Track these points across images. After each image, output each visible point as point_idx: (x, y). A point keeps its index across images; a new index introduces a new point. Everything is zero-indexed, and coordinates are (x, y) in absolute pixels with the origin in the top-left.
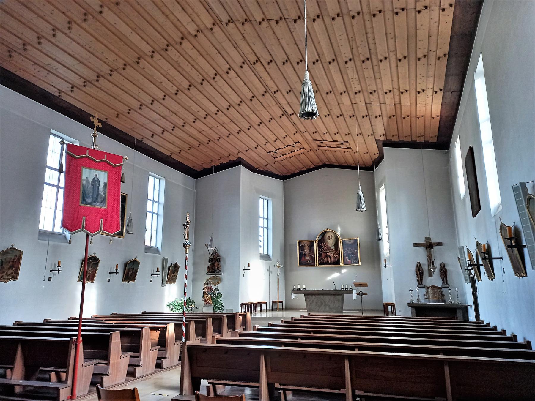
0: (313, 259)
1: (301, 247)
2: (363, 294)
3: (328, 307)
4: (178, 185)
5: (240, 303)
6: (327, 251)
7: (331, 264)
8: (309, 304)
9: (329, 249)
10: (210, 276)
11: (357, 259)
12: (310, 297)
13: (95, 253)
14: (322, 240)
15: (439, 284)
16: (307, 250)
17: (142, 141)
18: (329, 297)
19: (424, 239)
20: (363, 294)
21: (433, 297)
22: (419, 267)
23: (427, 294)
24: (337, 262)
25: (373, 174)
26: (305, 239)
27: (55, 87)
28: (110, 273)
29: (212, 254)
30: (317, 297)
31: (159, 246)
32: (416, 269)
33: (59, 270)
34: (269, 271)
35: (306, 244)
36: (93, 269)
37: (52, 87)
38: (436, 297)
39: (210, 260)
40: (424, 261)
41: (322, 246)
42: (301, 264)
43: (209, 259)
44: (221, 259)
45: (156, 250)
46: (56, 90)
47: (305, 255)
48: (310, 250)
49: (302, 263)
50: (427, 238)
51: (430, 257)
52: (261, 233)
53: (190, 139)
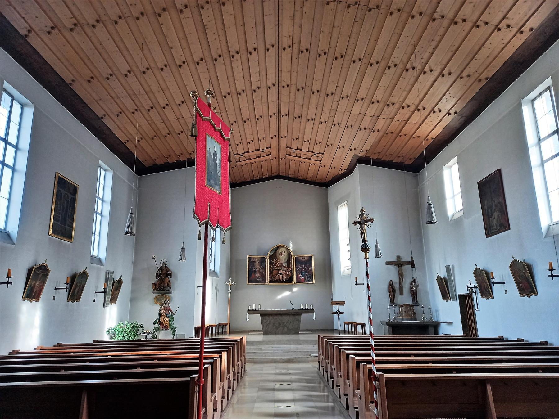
0: (263, 276)
1: (252, 263)
2: (340, 313)
3: (286, 328)
4: (124, 181)
7: (283, 282)
8: (265, 325)
9: (282, 265)
10: (155, 295)
11: (311, 276)
12: (267, 317)
13: (46, 261)
14: (274, 256)
15: (410, 302)
16: (257, 266)
17: (102, 118)
18: (288, 317)
19: (396, 258)
20: (340, 313)
21: (406, 315)
22: (391, 284)
23: (400, 312)
24: (290, 280)
25: (327, 190)
26: (254, 253)
27: (26, 21)
28: (56, 289)
30: (275, 317)
31: (103, 255)
32: (389, 287)
33: (8, 283)
34: (216, 288)
35: (256, 260)
36: (41, 282)
37: (22, 20)
38: (409, 315)
39: (157, 276)
40: (396, 280)
42: (250, 281)
43: (157, 274)
44: (173, 274)
45: (100, 261)
46: (26, 25)
47: (255, 271)
48: (260, 266)
49: (250, 281)
50: (398, 257)
51: (401, 276)
53: (161, 126)
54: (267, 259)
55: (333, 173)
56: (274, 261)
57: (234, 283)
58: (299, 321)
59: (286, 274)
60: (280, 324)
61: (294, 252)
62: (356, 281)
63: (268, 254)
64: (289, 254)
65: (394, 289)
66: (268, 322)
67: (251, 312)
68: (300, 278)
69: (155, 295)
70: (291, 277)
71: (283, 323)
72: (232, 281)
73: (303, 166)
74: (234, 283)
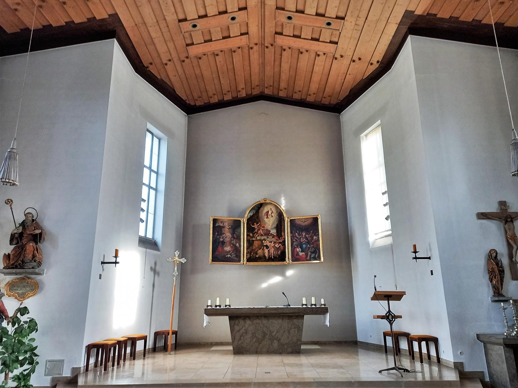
0: (237, 251)
2: (395, 317)
3: (275, 341)
5: (86, 343)
6: (263, 238)
7: (270, 259)
9: (267, 233)
10: (9, 278)
11: (316, 251)
12: (242, 322)
16: (227, 234)
18: (280, 321)
22: (493, 257)
24: (282, 257)
26: (223, 214)
29: (23, 224)
34: (154, 271)
39: (13, 238)
41: (254, 229)
42: (215, 259)
47: (223, 243)
48: (233, 234)
49: (215, 259)
50: (503, 204)
52: (144, 196)
54: (244, 221)
55: (351, 81)
56: (255, 226)
57: (183, 260)
58: (300, 329)
59: (274, 247)
60: (265, 334)
61: (287, 212)
62: (415, 252)
63: (246, 216)
64: (280, 215)
65: (502, 267)
66: (242, 331)
67: (211, 312)
68: (298, 254)
69: (9, 278)
70: (283, 253)
71: (271, 332)
72: (181, 257)
73: (304, 61)
74: (183, 260)
